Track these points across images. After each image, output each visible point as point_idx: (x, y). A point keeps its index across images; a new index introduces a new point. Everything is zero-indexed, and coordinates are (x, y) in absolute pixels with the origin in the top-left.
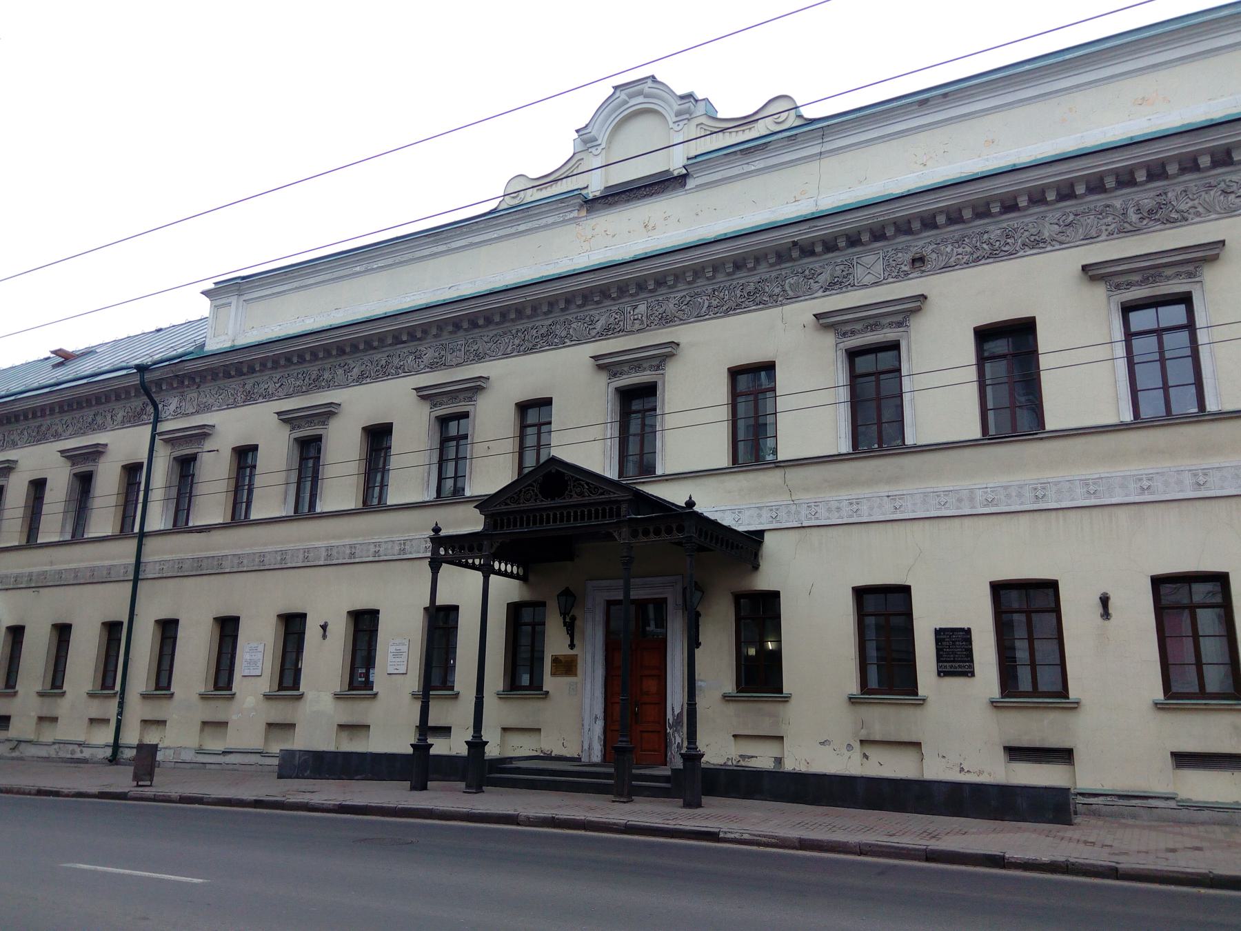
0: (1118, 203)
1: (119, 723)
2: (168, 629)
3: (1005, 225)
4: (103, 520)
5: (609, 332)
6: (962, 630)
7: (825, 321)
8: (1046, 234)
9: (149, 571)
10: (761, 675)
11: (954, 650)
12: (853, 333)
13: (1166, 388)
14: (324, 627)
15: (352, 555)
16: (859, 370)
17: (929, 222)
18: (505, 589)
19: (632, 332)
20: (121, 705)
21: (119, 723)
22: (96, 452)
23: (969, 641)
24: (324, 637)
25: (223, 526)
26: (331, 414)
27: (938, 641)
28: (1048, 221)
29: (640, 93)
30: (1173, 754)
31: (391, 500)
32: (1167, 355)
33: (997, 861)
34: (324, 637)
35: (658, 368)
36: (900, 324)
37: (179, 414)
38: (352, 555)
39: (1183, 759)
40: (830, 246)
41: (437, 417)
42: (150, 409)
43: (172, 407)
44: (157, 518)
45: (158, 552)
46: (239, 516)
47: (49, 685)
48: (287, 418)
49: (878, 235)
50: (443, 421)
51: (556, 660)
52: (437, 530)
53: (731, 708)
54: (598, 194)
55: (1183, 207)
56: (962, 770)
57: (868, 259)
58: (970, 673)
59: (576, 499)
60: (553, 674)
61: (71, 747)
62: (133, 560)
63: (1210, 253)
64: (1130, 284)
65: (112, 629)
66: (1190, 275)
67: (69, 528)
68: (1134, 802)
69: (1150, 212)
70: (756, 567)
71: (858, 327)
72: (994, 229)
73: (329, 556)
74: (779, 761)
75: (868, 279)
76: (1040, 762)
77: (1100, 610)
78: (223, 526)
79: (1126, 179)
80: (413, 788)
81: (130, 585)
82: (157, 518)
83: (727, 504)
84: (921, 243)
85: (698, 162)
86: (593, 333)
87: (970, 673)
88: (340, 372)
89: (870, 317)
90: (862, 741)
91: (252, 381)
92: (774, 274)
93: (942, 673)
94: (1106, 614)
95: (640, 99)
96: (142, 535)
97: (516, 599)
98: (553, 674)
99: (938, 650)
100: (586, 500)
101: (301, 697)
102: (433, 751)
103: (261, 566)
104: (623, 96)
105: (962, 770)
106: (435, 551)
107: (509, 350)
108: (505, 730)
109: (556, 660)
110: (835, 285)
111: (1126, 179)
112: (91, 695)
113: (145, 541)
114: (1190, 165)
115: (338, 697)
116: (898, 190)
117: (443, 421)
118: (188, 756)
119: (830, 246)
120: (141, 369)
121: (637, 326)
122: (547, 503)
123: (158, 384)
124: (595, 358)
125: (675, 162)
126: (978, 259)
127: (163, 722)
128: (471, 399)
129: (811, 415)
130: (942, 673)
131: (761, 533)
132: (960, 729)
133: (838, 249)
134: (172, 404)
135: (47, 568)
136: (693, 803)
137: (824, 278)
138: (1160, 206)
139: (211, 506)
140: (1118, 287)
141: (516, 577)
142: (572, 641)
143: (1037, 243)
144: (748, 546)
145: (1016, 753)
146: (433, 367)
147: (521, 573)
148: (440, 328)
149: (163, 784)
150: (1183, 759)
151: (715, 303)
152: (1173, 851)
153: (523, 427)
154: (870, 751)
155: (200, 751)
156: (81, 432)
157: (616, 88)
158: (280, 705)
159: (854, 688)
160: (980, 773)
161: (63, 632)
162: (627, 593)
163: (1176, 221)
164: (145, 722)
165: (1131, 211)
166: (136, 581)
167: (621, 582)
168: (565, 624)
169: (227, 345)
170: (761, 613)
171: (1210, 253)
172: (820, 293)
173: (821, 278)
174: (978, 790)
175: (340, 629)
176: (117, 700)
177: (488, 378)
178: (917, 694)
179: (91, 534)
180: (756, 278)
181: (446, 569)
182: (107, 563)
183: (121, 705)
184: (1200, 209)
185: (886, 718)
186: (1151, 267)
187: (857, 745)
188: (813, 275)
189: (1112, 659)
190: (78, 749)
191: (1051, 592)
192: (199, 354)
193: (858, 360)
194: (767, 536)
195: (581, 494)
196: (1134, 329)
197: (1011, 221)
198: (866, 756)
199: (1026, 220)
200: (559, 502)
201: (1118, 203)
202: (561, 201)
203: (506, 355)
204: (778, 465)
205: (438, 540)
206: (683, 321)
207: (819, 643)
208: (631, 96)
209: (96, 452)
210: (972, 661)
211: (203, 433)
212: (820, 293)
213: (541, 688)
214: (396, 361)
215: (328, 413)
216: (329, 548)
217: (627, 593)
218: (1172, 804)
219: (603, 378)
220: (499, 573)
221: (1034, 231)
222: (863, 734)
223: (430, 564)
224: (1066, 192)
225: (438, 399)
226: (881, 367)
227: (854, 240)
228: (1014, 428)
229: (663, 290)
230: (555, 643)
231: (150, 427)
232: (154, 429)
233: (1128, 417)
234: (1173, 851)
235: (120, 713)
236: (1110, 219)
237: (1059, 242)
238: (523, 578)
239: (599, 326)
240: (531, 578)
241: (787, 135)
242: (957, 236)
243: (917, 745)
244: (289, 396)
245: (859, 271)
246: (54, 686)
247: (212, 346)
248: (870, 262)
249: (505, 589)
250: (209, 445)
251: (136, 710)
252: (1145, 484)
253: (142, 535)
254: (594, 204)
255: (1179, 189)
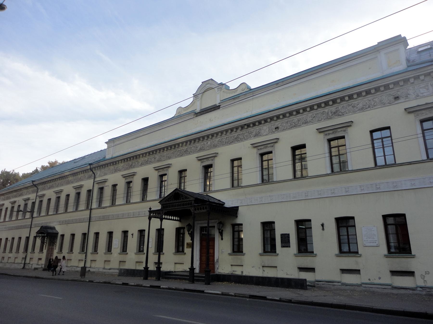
0: (326, 111)
1: (85, 261)
2: (97, 234)
3: (298, 118)
4: (82, 206)
5: (201, 150)
6: (287, 234)
7: (320, 131)
8: (308, 120)
9: (93, 219)
10: (237, 248)
11: (285, 239)
12: (261, 149)
13: (385, 156)
14: (132, 235)
15: (139, 214)
16: (425, 128)
17: (278, 117)
18: (177, 224)
19: (206, 150)
20: (86, 256)
21: (85, 261)
22: (81, 187)
23: (289, 237)
24: (323, 229)
25: (110, 207)
26: (82, 187)
27: (281, 237)
28: (308, 116)
29: (209, 83)
30: (340, 269)
31: (148, 199)
32: (385, 146)
33: (264, 298)
34: (323, 229)
35: (213, 160)
36: (272, 146)
37: (100, 176)
38: (139, 214)
39: (344, 271)
40: (254, 124)
41: (203, 166)
42: (93, 175)
43: (98, 174)
44: (95, 205)
45: (96, 213)
46: (113, 203)
47: (122, 251)
48: (124, 177)
49: (266, 121)
50: (262, 155)
51: (187, 244)
52: (150, 209)
53: (231, 257)
54: (199, 111)
55: (343, 111)
56: (287, 274)
57: (265, 128)
58: (289, 246)
59: (181, 201)
60: (187, 248)
61: (74, 268)
62: (89, 216)
63: (349, 125)
64: (329, 134)
65: (84, 234)
66: (345, 131)
67: (75, 208)
68: (330, 283)
69: (334, 113)
70: (237, 217)
71: (262, 147)
72: (295, 119)
73: (133, 215)
74: (242, 272)
75: (265, 134)
76: (307, 272)
77: (322, 228)
78: (110, 207)
79: (326, 104)
80: (206, 284)
81: (29, 229)
82: (95, 205)
83: (229, 200)
84: (277, 123)
85: (223, 101)
86: (197, 150)
87: (289, 246)
88: (137, 163)
89: (265, 144)
90: (263, 267)
91: (342, 106)
92: (241, 133)
93: (283, 246)
94: (323, 229)
95: (209, 85)
96: (91, 209)
97: (178, 227)
98: (187, 248)
99: (281, 240)
100: (184, 200)
101: (127, 254)
102: (149, 269)
103: (118, 217)
104: (204, 84)
105: (287, 274)
106: (150, 214)
107: (320, 119)
108: (175, 263)
109: (187, 244)
110: (256, 135)
111: (326, 104)
112: (79, 253)
113: (92, 211)
114: (342, 99)
115: (120, 254)
116: (272, 109)
117: (262, 155)
118: (101, 270)
119: (254, 124)
120: (90, 164)
121: (208, 148)
122: (175, 201)
123: (95, 168)
124: (405, 109)
125: (217, 102)
126: (291, 128)
127: (95, 261)
128: (167, 170)
129: (250, 174)
130: (283, 246)
131: (238, 207)
132: (286, 263)
133: (250, 127)
134: (98, 173)
135: (70, 219)
136: (146, 278)
137: (254, 133)
138: (337, 111)
139: (107, 202)
140: (326, 135)
141: (177, 220)
142: (222, 237)
143: (306, 123)
144: (234, 211)
145: (301, 269)
146: (159, 161)
147: (179, 219)
148: (124, 160)
149: (88, 278)
150: (344, 271)
151: (227, 141)
152: (325, 296)
153: (233, 167)
154: (265, 269)
155: (104, 268)
156: (57, 186)
157: (202, 82)
158: (122, 256)
159: (260, 250)
160: (292, 275)
161: (110, 234)
162: (208, 224)
163: (239, 141)
164: (91, 261)
165: (330, 113)
166: (90, 222)
167: (207, 221)
168: (219, 232)
169: (110, 157)
170: (237, 229)
171: (349, 125)
172: (253, 138)
173: (253, 134)
174: (251, 278)
175: (136, 235)
176: (85, 255)
177: (171, 164)
178: (411, 253)
179: (13, 219)
180: (237, 134)
181: (153, 219)
182: (83, 217)
183: (86, 256)
184: (347, 112)
185: (269, 259)
186: (334, 129)
187: (261, 267)
188: (251, 133)
189: (325, 240)
190: (76, 268)
191: (403, 217)
192: (104, 159)
193: (374, 134)
194: (239, 208)
195: (183, 199)
196: (425, 128)
197: (299, 117)
198: (264, 271)
199: (303, 116)
200: (178, 201)
201: (326, 111)
202: (189, 114)
203: (176, 157)
204: (242, 187)
205: (151, 211)
206: (219, 147)
207: (252, 237)
208: (206, 84)
209: (81, 187)
210: (290, 243)
211: (105, 181)
212: (253, 138)
213: (184, 252)
214: (150, 160)
215: (133, 175)
216: (133, 213)
217: (208, 224)
218: (340, 284)
219: (199, 162)
220: (165, 219)
221: (305, 119)
222: (263, 264)
223: (149, 218)
224: (312, 108)
225: (159, 170)
226: (340, 144)
227: (260, 123)
228: (332, 171)
229: (273, 122)
230: (188, 239)
231: (93, 180)
232: (94, 180)
233: (425, 158)
234: (325, 296)
235: (86, 258)
236: (324, 115)
237: (311, 122)
238: (179, 221)
239: (198, 148)
240: (182, 220)
241: (246, 93)
242: (286, 121)
243: (276, 267)
244: (125, 170)
245: (262, 131)
246: (123, 251)
247: (108, 157)
248: (265, 128)
249: (177, 224)
250: (107, 184)
251: (90, 257)
252: (333, 191)
253: (91, 209)
254: (198, 114)
255: (342, 106)
